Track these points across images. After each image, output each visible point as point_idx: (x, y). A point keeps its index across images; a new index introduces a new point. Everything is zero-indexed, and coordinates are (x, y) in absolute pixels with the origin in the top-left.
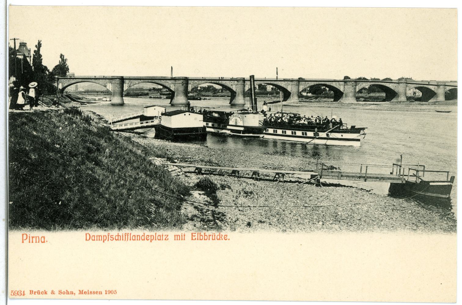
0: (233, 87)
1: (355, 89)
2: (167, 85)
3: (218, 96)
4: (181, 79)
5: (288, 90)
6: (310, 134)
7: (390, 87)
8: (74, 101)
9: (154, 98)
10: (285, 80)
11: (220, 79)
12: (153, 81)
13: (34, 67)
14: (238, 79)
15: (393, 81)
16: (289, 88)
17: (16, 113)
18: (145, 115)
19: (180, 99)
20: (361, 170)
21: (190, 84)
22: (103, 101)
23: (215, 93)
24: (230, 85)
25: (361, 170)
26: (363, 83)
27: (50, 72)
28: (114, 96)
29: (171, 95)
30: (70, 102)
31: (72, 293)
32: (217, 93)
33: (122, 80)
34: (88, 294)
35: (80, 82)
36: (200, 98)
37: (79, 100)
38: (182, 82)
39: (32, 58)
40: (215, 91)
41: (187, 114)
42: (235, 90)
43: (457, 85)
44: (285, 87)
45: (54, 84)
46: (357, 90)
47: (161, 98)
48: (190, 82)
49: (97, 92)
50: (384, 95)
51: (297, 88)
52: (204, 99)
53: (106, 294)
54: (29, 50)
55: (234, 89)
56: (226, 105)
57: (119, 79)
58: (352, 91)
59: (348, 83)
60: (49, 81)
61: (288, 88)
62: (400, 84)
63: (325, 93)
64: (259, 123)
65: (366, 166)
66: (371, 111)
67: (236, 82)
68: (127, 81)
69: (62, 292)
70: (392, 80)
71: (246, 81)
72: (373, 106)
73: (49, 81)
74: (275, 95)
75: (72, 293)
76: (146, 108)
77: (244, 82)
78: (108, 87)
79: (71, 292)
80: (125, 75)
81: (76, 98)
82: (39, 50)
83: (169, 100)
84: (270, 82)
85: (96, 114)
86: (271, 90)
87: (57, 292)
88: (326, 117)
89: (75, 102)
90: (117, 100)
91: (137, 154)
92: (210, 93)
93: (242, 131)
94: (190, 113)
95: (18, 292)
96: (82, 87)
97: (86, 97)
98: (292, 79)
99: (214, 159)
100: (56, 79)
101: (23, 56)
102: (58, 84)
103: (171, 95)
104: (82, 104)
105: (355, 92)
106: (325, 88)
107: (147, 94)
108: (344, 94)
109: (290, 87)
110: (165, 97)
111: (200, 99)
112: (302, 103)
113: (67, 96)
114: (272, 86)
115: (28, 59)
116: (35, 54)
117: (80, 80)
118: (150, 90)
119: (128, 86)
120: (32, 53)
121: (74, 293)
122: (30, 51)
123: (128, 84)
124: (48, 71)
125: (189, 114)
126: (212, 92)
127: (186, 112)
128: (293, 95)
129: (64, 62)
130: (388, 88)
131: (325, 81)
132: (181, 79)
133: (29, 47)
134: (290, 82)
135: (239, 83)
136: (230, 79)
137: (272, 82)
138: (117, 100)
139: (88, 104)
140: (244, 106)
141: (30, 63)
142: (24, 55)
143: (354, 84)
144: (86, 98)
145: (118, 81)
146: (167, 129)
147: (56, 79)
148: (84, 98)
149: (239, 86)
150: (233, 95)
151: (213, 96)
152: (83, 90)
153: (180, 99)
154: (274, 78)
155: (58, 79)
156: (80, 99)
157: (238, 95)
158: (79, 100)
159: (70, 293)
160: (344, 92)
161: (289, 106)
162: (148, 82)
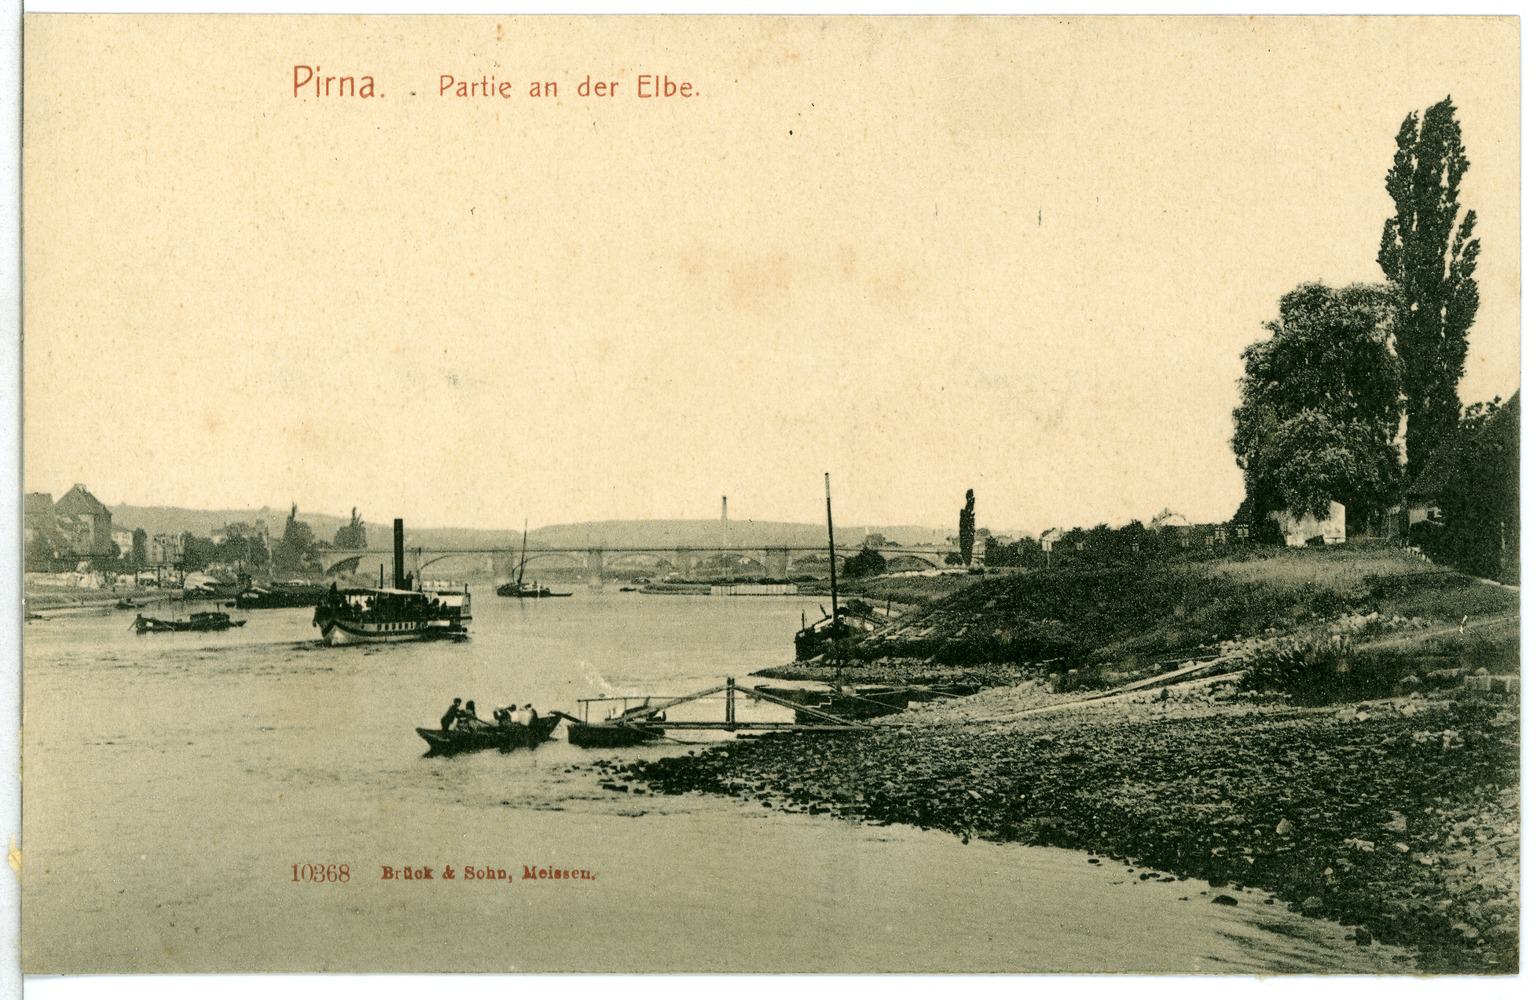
13: (255, 599)
31: (502, 874)
34: (551, 877)
53: (296, 879)
69: (475, 872)
75: (502, 874)
79: (499, 872)
87: (460, 873)
88: (1449, 96)
91: (1402, 943)
95: (314, 871)
99: (976, 565)
121: (507, 876)
154: (935, 524)
159: (497, 875)
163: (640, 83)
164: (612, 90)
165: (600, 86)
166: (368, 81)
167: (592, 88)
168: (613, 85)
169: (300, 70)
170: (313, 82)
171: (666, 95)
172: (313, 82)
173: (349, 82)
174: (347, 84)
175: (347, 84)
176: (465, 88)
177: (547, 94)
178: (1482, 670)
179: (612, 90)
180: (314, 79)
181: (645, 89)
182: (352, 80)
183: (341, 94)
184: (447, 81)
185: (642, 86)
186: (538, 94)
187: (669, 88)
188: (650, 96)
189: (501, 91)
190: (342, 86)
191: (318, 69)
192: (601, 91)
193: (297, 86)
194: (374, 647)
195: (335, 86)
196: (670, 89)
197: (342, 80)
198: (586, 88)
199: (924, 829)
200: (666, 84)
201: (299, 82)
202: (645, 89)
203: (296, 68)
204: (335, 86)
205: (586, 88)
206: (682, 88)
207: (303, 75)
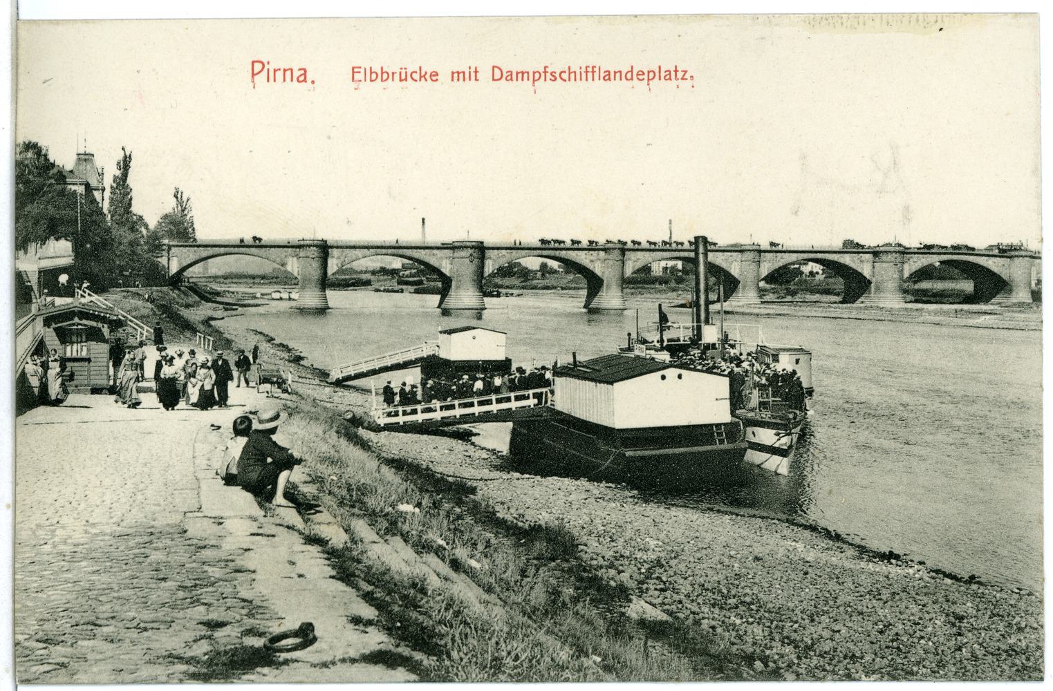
0: (596, 265)
1: (901, 271)
2: (433, 261)
3: (535, 288)
4: (466, 247)
5: (733, 273)
8: (208, 300)
9: (385, 291)
11: (518, 245)
12: (400, 252)
15: (976, 252)
16: (735, 267)
18: (441, 356)
19: (464, 296)
21: (490, 258)
22: (273, 299)
23: (527, 280)
24: (588, 261)
26: (921, 256)
28: (303, 288)
29: (445, 285)
30: (197, 304)
32: (532, 280)
33: (324, 249)
35: (223, 255)
36: (497, 291)
37: (219, 299)
38: (471, 255)
39: (107, 194)
40: (525, 274)
41: (671, 373)
42: (599, 274)
44: (724, 265)
45: (159, 259)
46: (906, 275)
47: (402, 291)
48: (489, 253)
49: (253, 277)
50: (968, 286)
52: (507, 295)
54: (100, 171)
55: (598, 271)
56: (576, 310)
57: (316, 246)
58: (895, 276)
59: (884, 257)
60: (150, 251)
62: (1016, 259)
63: (800, 281)
66: (991, 331)
67: (602, 254)
68: (335, 252)
70: (863, 247)
71: (627, 253)
72: (988, 317)
73: (150, 251)
74: (673, 284)
76: (445, 335)
77: (623, 255)
78: (289, 268)
80: (330, 236)
81: (210, 293)
82: (125, 175)
83: (437, 298)
84: (814, 256)
85: (274, 342)
86: (661, 274)
89: (210, 304)
90: (311, 298)
92: (514, 281)
94: (683, 372)
96: (217, 266)
97: (231, 290)
100: (164, 247)
101: (84, 187)
102: (169, 259)
103: (445, 285)
104: (226, 310)
105: (901, 278)
106: (799, 268)
107: (367, 283)
108: (872, 285)
109: (738, 267)
110: (412, 288)
111: (498, 295)
112: (774, 306)
113: (191, 288)
115: (97, 195)
116: (115, 185)
117: (222, 250)
118: (374, 273)
119: (337, 265)
120: (108, 182)
122: (101, 174)
123: (339, 258)
124: (146, 226)
125: (680, 377)
126: (518, 277)
127: (665, 366)
128: (744, 287)
129: (182, 206)
130: (983, 267)
131: (412, 248)
132: (466, 247)
133: (99, 161)
134: (736, 254)
135: (610, 257)
138: (311, 298)
139: (240, 309)
140: (621, 315)
141: (100, 205)
142: (87, 186)
143: (899, 260)
144: (233, 293)
145: (314, 252)
146: (561, 421)
147: (164, 247)
148: (228, 292)
149: (611, 263)
150: (594, 284)
151: (524, 288)
152: (220, 273)
153: (464, 296)
155: (170, 247)
156: (218, 294)
157: (608, 287)
158: (219, 299)
160: (874, 280)
161: (737, 313)
162: (387, 255)
163: (353, 72)
166: (302, 72)
167: (635, 73)
169: (255, 64)
171: (371, 81)
174: (288, 73)
175: (288, 73)
177: (593, 80)
180: (265, 70)
182: (292, 70)
184: (258, 67)
190: (284, 75)
191: (268, 63)
192: (641, 77)
193: (253, 75)
194: (795, 323)
195: (279, 75)
197: (285, 70)
198: (457, 75)
200: (371, 73)
201: (255, 72)
203: (253, 62)
204: (279, 75)
205: (457, 75)
207: (258, 67)
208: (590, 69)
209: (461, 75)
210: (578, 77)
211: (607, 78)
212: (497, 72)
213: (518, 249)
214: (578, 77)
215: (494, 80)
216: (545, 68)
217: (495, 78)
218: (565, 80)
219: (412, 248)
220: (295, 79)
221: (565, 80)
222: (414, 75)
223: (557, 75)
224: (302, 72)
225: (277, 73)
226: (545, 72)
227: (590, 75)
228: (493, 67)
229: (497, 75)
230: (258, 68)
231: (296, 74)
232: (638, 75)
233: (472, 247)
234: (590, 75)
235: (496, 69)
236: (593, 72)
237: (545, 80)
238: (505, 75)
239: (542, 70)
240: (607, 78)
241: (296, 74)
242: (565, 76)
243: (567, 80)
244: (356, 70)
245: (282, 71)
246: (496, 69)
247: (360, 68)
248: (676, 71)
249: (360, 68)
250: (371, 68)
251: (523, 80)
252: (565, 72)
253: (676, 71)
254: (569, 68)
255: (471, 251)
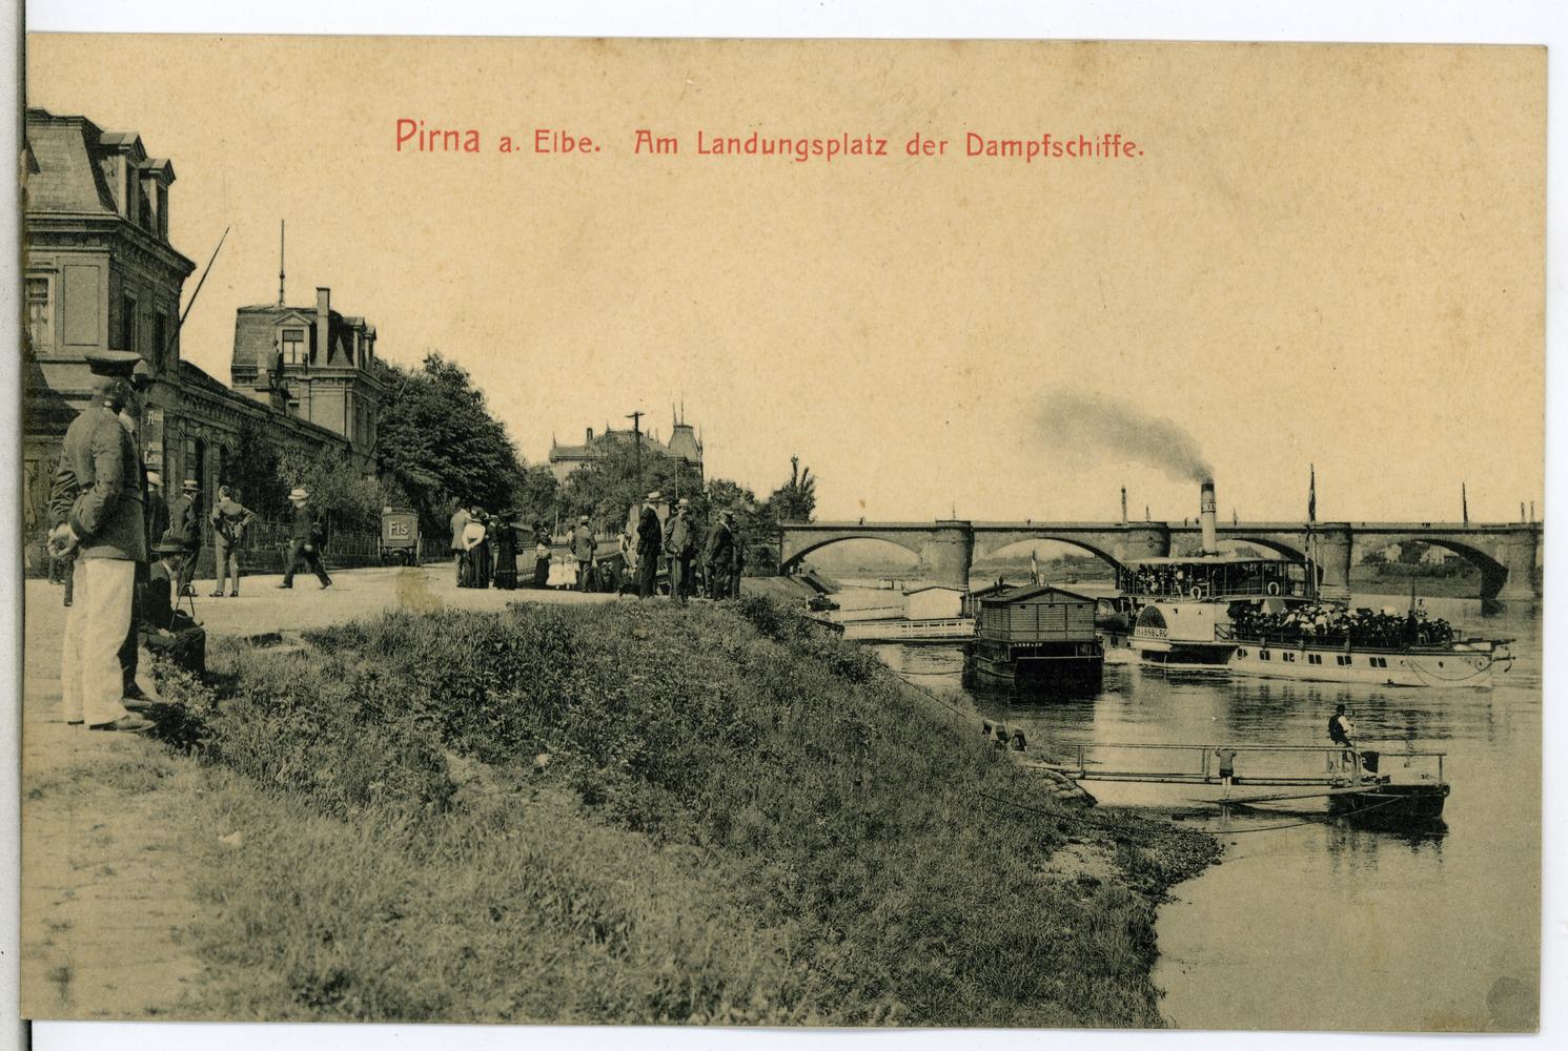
6: (1329, 657)
7: (1476, 547)
10: (1486, 530)
14: (1330, 526)
17: (594, 604)
20: (1441, 763)
25: (1441, 763)
27: (391, 376)
33: (968, 531)
43: (1220, 535)
48: (1174, 536)
51: (1529, 552)
61: (1495, 554)
64: (1216, 633)
65: (61, 270)
80: (977, 515)
86: (1443, 562)
93: (1167, 653)
98: (1510, 524)
114: (1447, 552)
131: (1091, 530)
136: (1113, 526)
137: (1447, 537)
163: (538, 138)
164: (942, 148)
165: (929, 144)
166: (473, 136)
168: (942, 144)
169: (404, 125)
170: (416, 138)
172: (416, 138)
173: (787, 143)
174: (452, 139)
175: (452, 139)
176: (722, 145)
178: (690, 598)
179: (942, 148)
180: (417, 134)
181: (543, 145)
183: (637, 151)
184: (406, 129)
185: (540, 141)
186: (860, 152)
187: (567, 143)
188: (547, 151)
189: (925, 150)
191: (422, 123)
192: (585, 148)
193: (400, 140)
195: (439, 140)
196: (568, 144)
197: (447, 134)
198: (669, 144)
199: (1157, 936)
200: (565, 140)
201: (402, 136)
202: (543, 145)
203: (400, 122)
204: (439, 140)
205: (669, 144)
206: (581, 144)
208: (1111, 140)
209: (1016, 147)
210: (1094, 151)
211: (857, 150)
212: (975, 143)
213: (1191, 530)
214: (1094, 151)
215: (969, 153)
216: (1046, 136)
217: (972, 151)
218: (1074, 155)
219: (1091, 530)
220: (461, 145)
221: (1074, 155)
222: (1072, 148)
223: (1064, 148)
224: (473, 136)
225: (436, 137)
226: (1046, 143)
227: (1112, 148)
228: (969, 135)
229: (975, 147)
230: (406, 130)
231: (464, 139)
232: (925, 147)
233: (1151, 529)
234: (1112, 148)
235: (972, 138)
236: (1107, 143)
237: (1046, 154)
238: (986, 147)
239: (1041, 139)
240: (857, 150)
241: (464, 139)
242: (1075, 148)
243: (1078, 154)
244: (541, 135)
245: (443, 134)
246: (972, 138)
247: (548, 131)
248: (869, 141)
249: (548, 131)
250: (564, 133)
251: (1012, 154)
252: (1074, 143)
253: (869, 141)
254: (1081, 137)
255: (1151, 534)
